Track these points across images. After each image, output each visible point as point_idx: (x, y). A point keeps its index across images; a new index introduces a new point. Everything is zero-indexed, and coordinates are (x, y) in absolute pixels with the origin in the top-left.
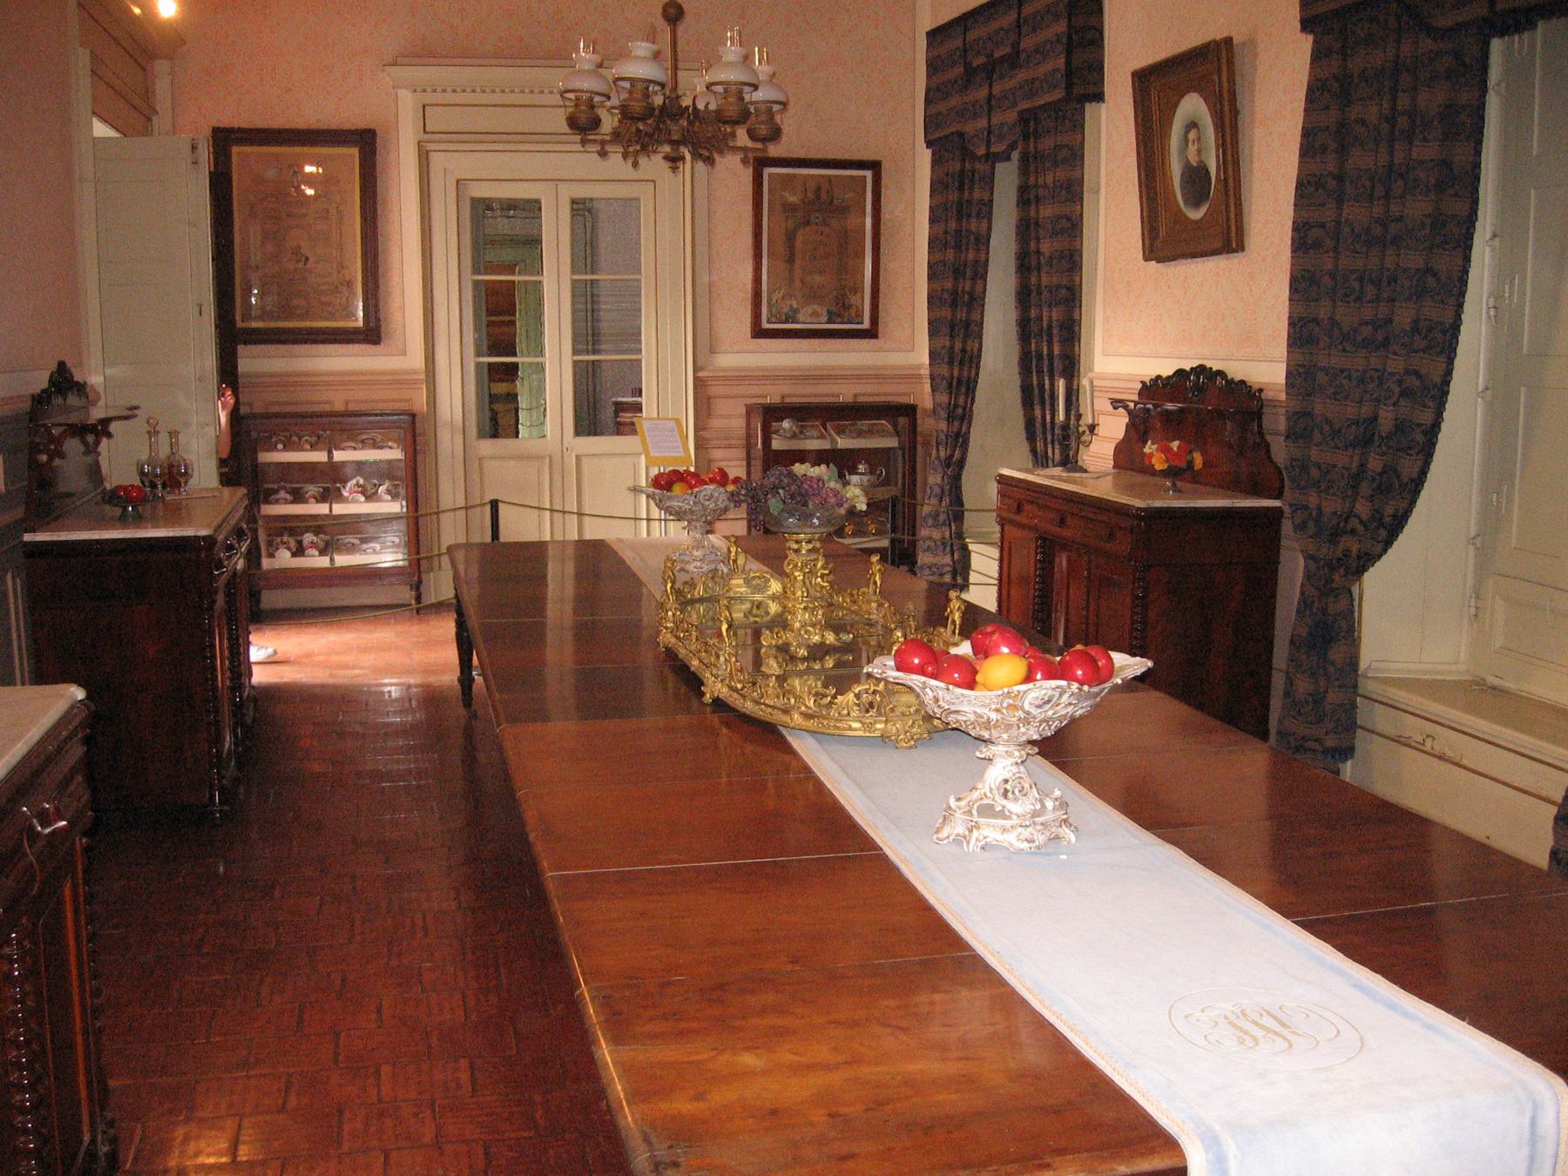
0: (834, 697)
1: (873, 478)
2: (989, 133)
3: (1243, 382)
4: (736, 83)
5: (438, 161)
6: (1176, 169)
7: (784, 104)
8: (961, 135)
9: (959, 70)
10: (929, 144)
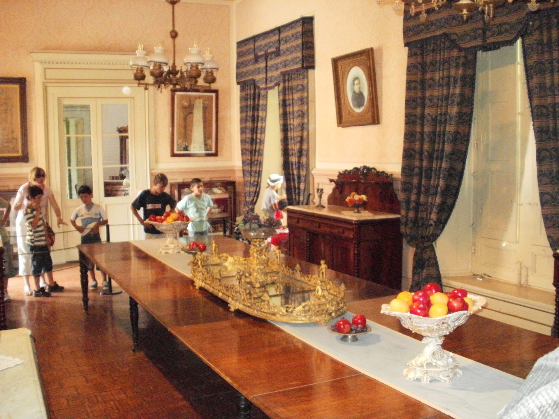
0: (294, 308)
1: (220, 209)
2: (266, 80)
3: (383, 172)
4: (196, 63)
5: (50, 90)
6: (349, 95)
7: (217, 69)
8: (254, 80)
9: (252, 56)
10: (238, 83)
